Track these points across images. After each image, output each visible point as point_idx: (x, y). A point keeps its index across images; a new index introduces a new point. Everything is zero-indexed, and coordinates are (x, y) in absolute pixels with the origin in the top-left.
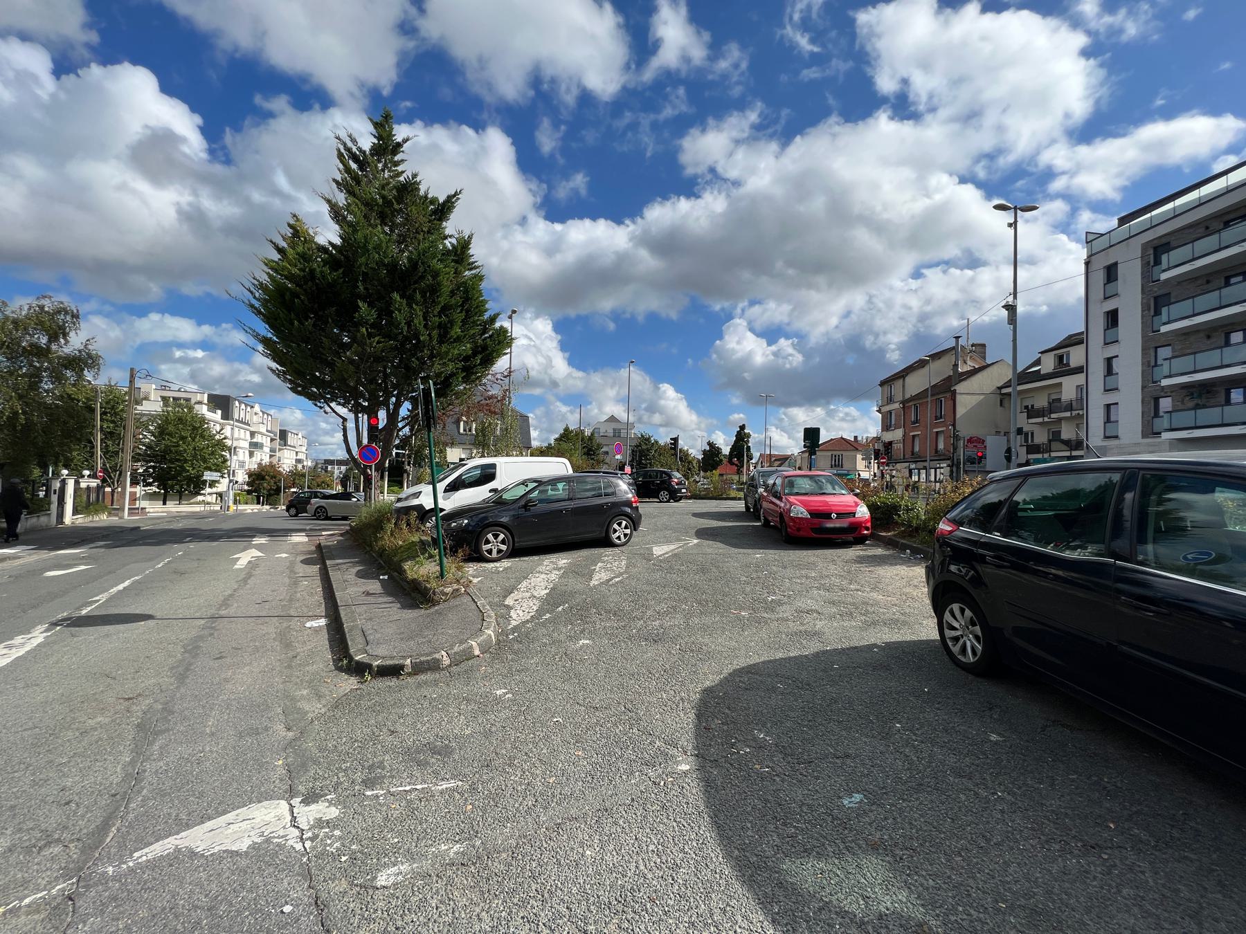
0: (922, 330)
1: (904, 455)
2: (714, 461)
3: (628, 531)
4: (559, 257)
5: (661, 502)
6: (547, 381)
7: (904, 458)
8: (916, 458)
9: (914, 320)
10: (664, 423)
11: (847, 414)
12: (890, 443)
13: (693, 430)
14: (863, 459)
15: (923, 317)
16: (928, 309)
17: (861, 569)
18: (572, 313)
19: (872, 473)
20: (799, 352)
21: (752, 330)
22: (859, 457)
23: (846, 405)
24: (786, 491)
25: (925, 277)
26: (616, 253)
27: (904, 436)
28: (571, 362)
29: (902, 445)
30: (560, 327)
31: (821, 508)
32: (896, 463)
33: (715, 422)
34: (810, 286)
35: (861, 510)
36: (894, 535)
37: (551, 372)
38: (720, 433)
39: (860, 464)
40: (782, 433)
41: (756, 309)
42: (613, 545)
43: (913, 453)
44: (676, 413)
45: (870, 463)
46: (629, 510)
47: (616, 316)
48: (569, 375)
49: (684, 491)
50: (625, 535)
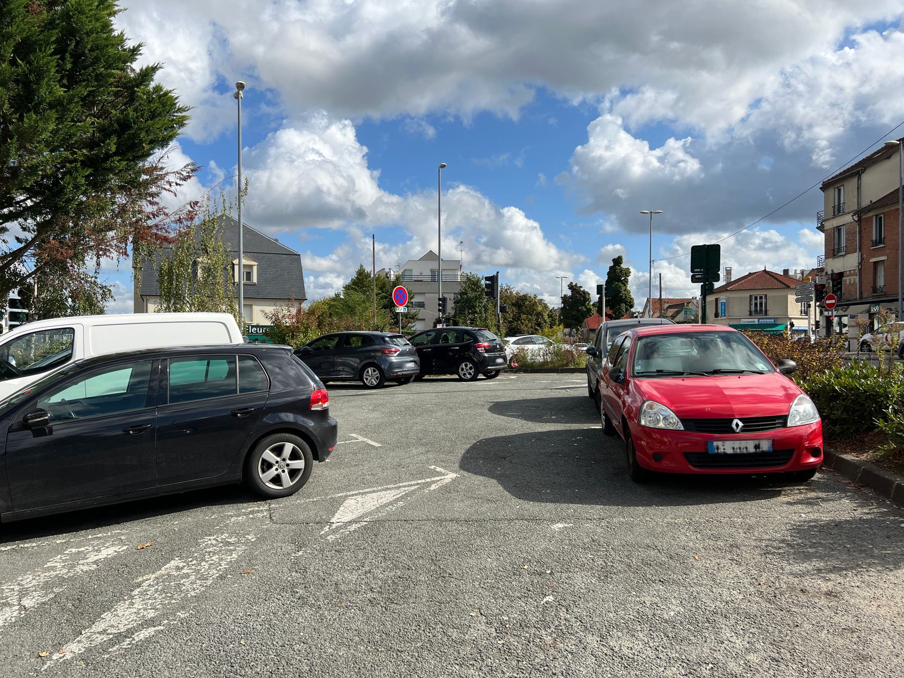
0: (863, 119)
1: (861, 293)
2: (579, 311)
3: (299, 464)
4: (350, 40)
5: (460, 380)
6: (349, 209)
7: (861, 298)
8: (879, 296)
9: (849, 106)
10: (511, 262)
11: (765, 240)
12: (841, 275)
13: (551, 271)
14: (797, 301)
15: (862, 103)
16: (866, 89)
17: (807, 583)
18: (376, 115)
19: (812, 322)
20: (693, 156)
21: (627, 129)
22: (792, 298)
23: (763, 230)
24: (638, 368)
25: (858, 44)
26: (429, 31)
27: (860, 264)
28: (382, 184)
29: (857, 278)
30: (364, 134)
31: (708, 407)
32: (849, 305)
33: (582, 258)
34: (703, 65)
35: (801, 408)
36: (877, 462)
37: (352, 197)
38: (591, 273)
39: (794, 308)
40: (678, 269)
41: (630, 101)
42: (263, 496)
43: (875, 289)
44: (528, 247)
45: (809, 306)
46: (289, 417)
47: (433, 118)
48: (379, 201)
49: (500, 361)
50: (293, 473)
